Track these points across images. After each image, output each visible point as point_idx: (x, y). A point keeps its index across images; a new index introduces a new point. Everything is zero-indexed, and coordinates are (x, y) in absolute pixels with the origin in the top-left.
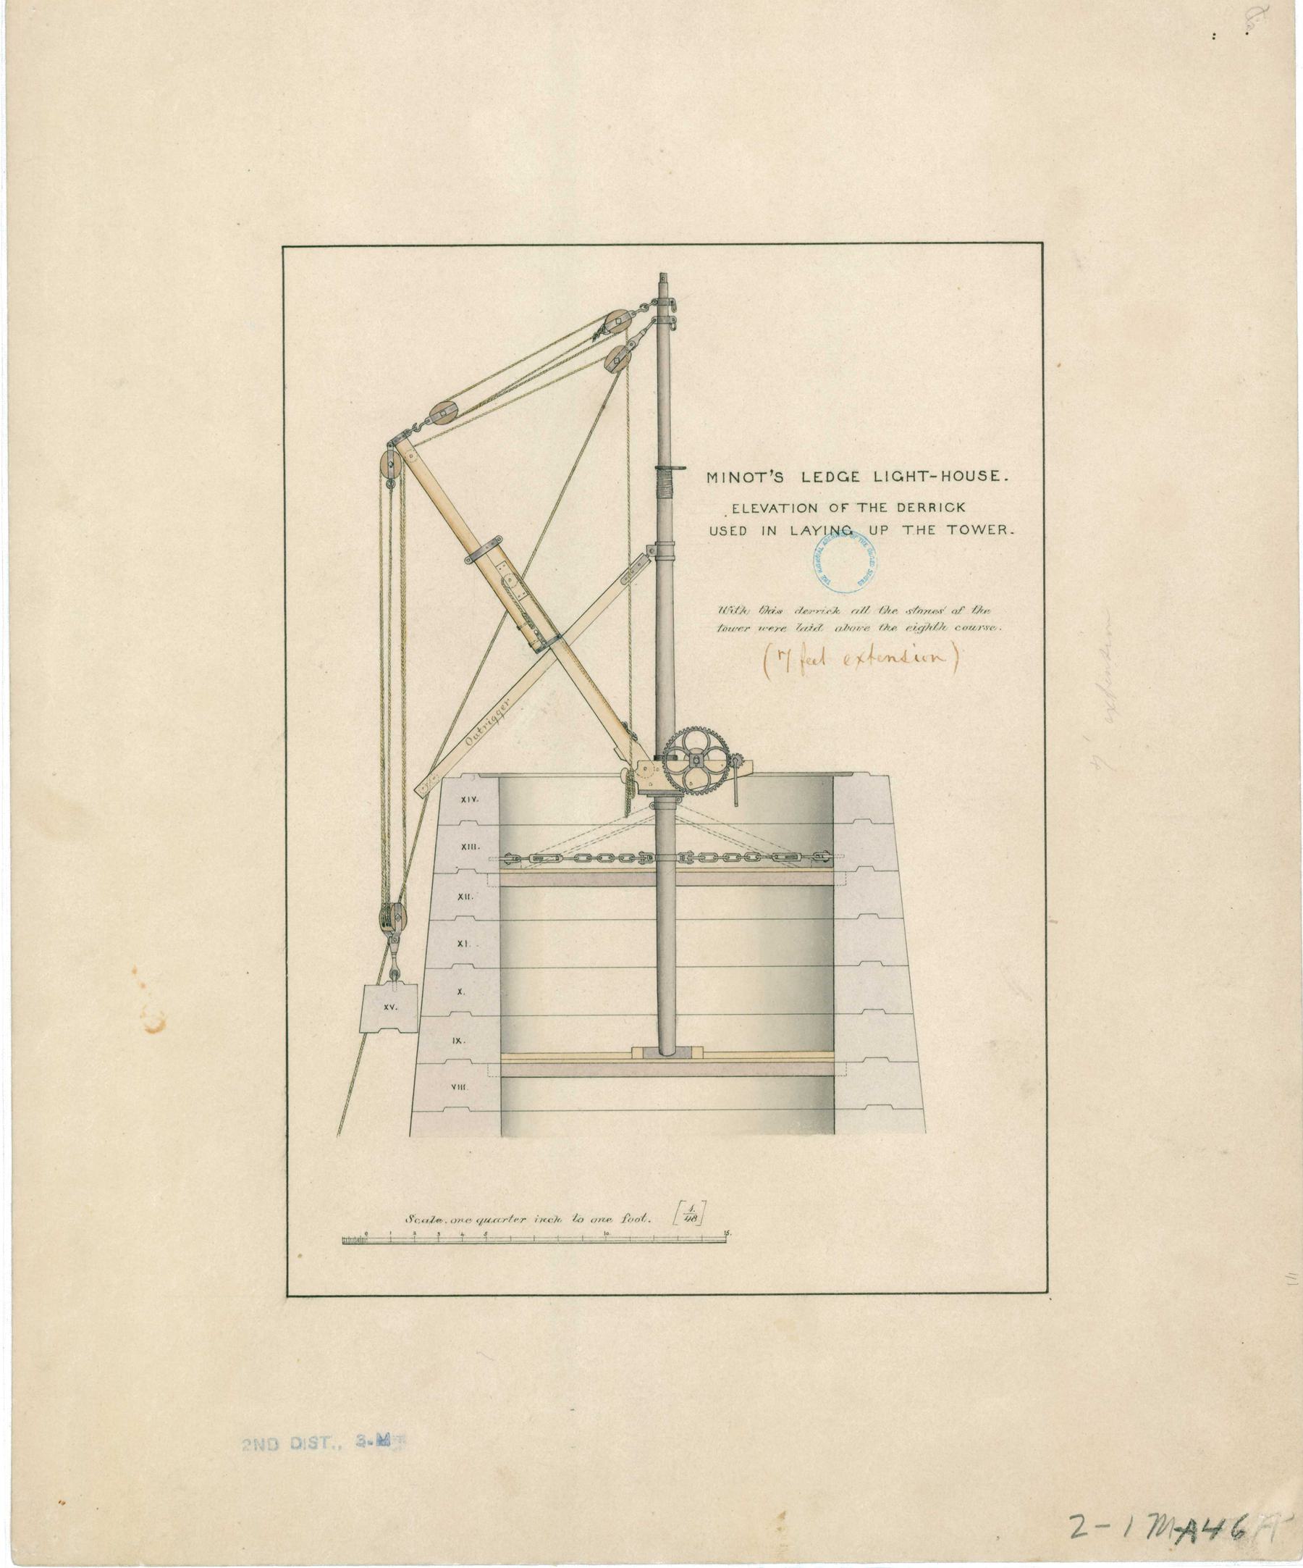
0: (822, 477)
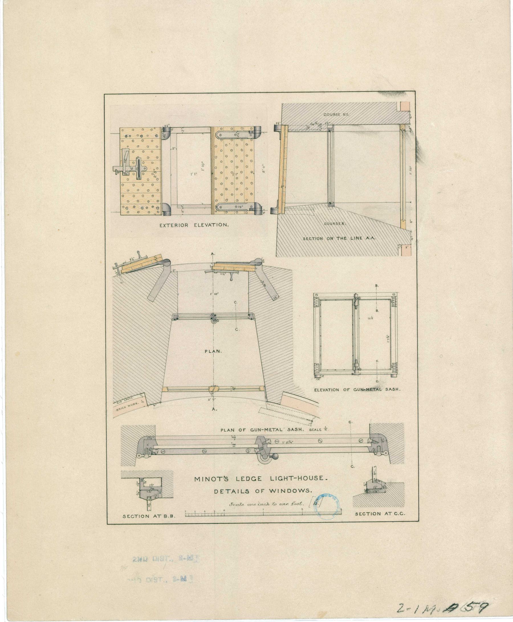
0: (245, 479)
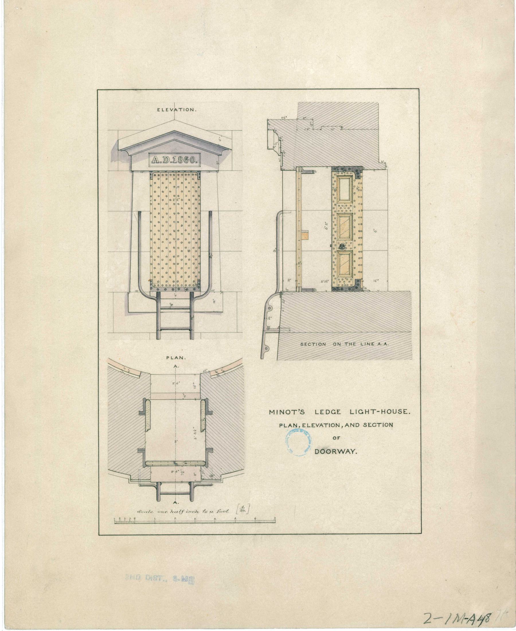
0: (324, 412)
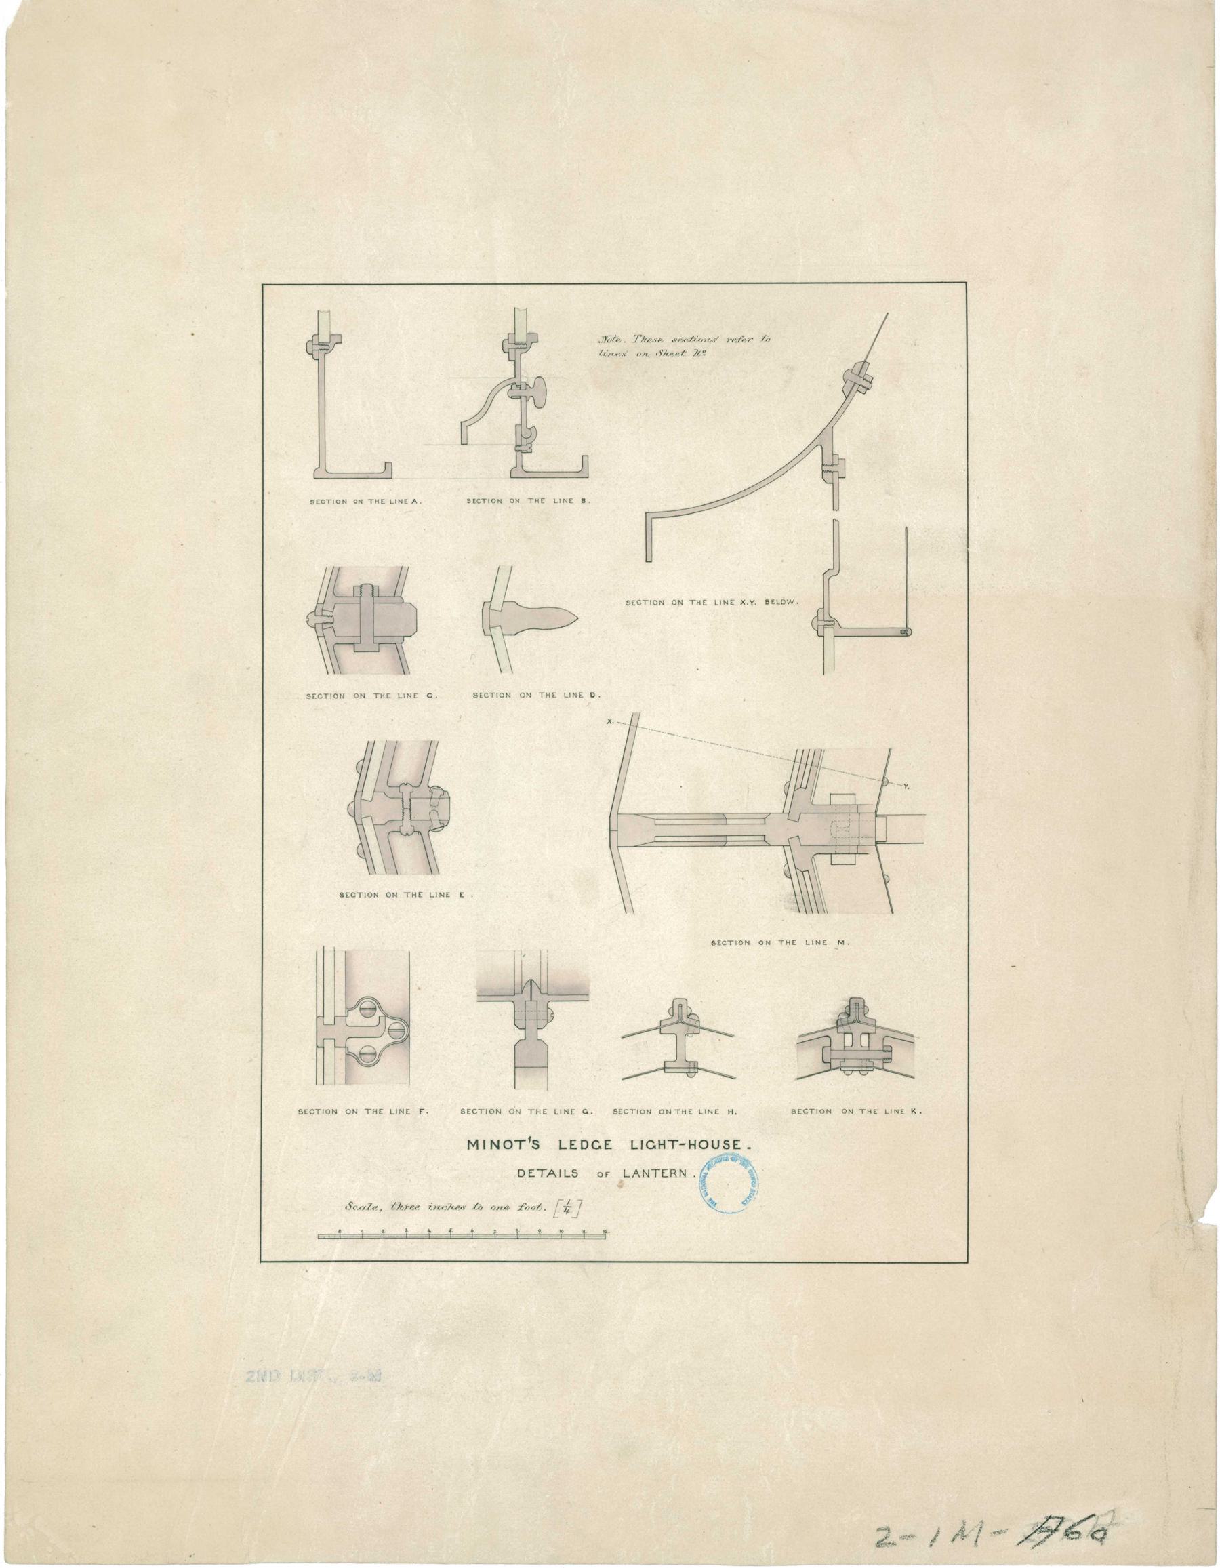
0: (577, 1144)
